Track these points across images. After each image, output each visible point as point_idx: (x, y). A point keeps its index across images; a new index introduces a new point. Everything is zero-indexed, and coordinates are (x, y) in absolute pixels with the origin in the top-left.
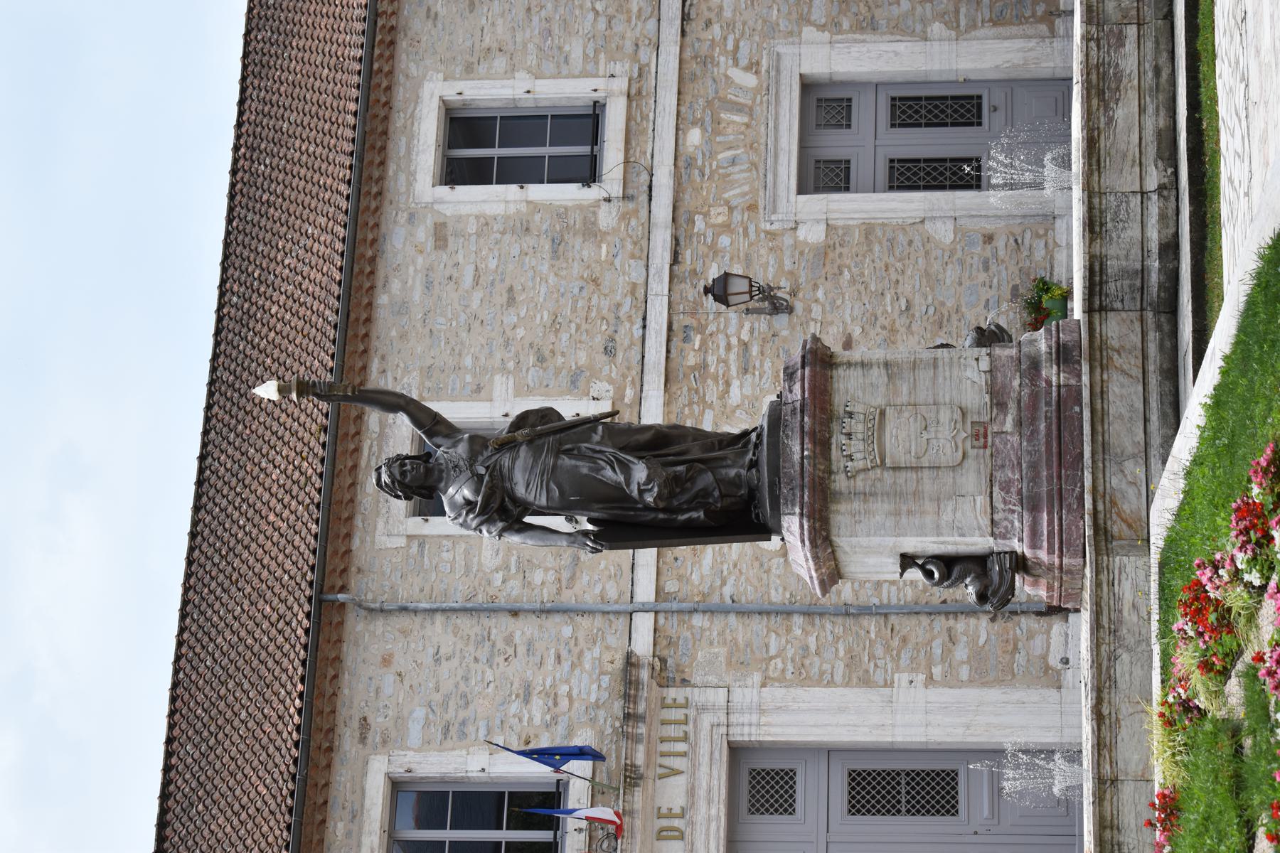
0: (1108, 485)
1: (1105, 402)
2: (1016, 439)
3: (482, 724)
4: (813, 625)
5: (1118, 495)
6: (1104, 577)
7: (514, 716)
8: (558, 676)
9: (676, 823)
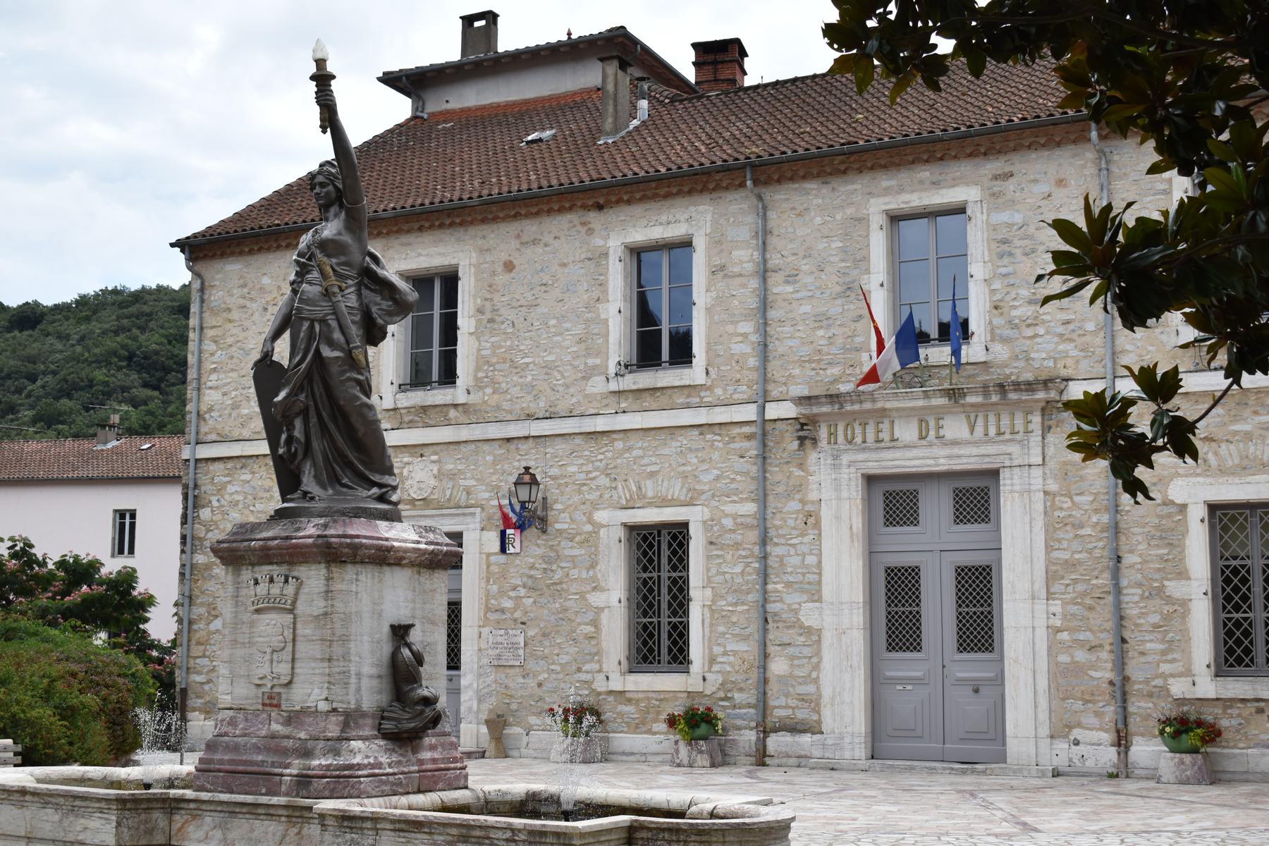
0: (208, 813)
1: (265, 817)
2: (264, 733)
3: (1010, 269)
4: (1102, 532)
5: (199, 822)
6: (103, 805)
7: (1017, 294)
8: (1052, 324)
9: (932, 433)
